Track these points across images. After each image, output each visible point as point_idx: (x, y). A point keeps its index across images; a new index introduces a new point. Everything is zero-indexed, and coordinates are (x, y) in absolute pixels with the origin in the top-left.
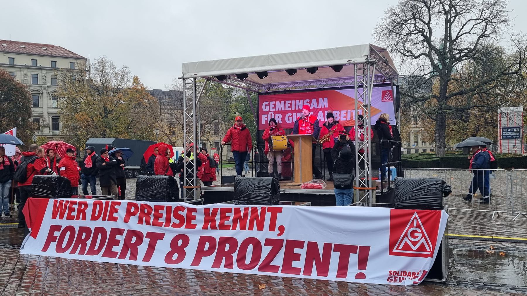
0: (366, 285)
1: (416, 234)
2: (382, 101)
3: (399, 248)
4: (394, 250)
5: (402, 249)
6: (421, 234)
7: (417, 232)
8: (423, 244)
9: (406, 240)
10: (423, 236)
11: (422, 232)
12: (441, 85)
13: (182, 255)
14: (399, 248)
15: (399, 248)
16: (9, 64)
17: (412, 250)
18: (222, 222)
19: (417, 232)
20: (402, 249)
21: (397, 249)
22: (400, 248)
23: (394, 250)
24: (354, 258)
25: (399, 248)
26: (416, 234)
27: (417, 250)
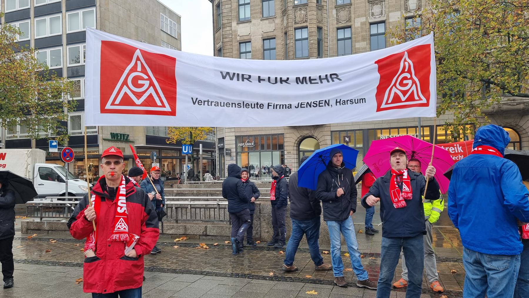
0: (211, 129)
1: (140, 82)
2: (103, 110)
3: (388, 102)
4: (108, 106)
5: (392, 102)
6: (148, 82)
7: (143, 79)
8: (151, 96)
9: (125, 89)
10: (152, 84)
11: (150, 79)
12: (274, 235)
13: (281, 231)
14: (115, 103)
15: (388, 102)
16: (52, 198)
17: (134, 104)
18: (150, 216)
19: (143, 79)
20: (120, 104)
21: (113, 104)
22: (117, 101)
23: (382, 107)
24: (364, 100)
25: (115, 103)
26: (140, 82)
27: (141, 105)
